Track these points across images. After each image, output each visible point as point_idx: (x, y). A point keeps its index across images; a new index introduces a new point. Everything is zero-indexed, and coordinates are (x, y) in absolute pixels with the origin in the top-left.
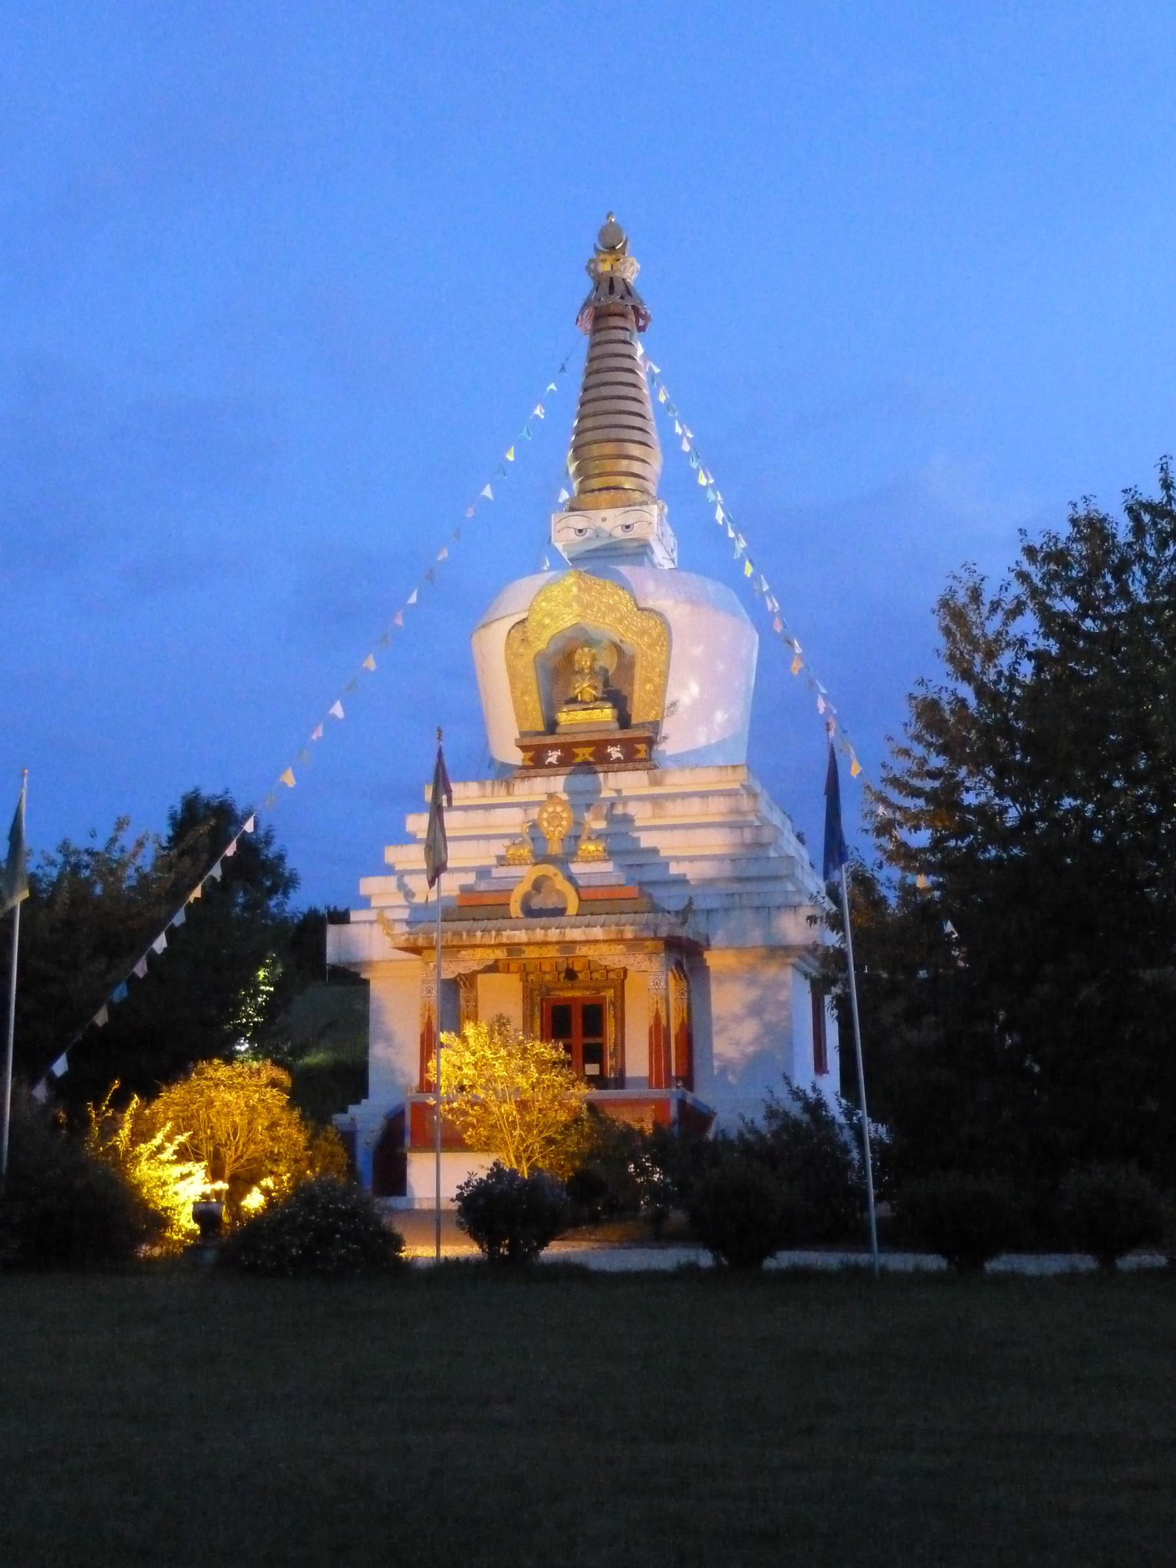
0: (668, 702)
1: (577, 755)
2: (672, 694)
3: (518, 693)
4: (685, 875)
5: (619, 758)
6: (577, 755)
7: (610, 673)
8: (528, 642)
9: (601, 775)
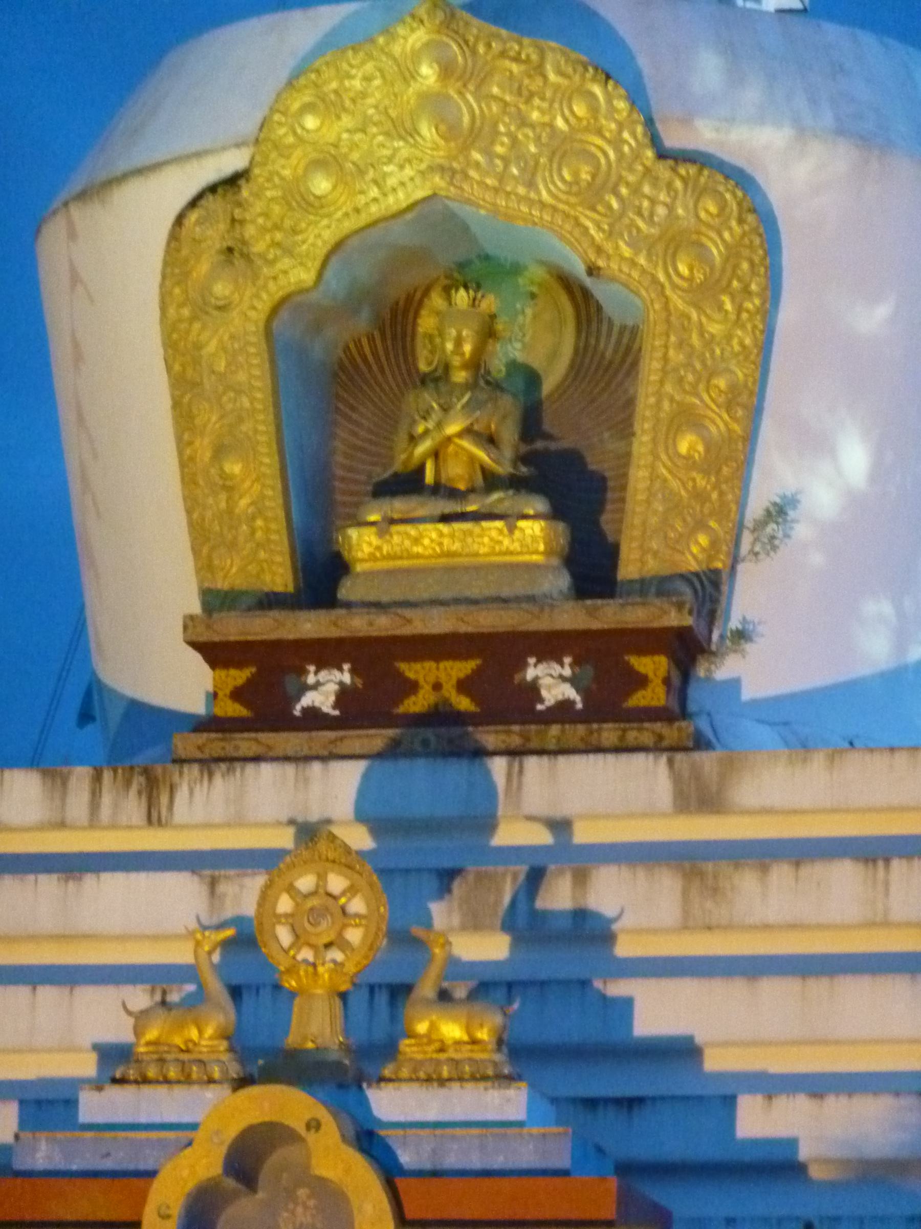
0: (755, 508)
1: (412, 687)
2: (775, 472)
3: (203, 449)
4: (792, 1143)
5: (565, 705)
6: (412, 687)
7: (548, 385)
8: (247, 258)
9: (498, 766)
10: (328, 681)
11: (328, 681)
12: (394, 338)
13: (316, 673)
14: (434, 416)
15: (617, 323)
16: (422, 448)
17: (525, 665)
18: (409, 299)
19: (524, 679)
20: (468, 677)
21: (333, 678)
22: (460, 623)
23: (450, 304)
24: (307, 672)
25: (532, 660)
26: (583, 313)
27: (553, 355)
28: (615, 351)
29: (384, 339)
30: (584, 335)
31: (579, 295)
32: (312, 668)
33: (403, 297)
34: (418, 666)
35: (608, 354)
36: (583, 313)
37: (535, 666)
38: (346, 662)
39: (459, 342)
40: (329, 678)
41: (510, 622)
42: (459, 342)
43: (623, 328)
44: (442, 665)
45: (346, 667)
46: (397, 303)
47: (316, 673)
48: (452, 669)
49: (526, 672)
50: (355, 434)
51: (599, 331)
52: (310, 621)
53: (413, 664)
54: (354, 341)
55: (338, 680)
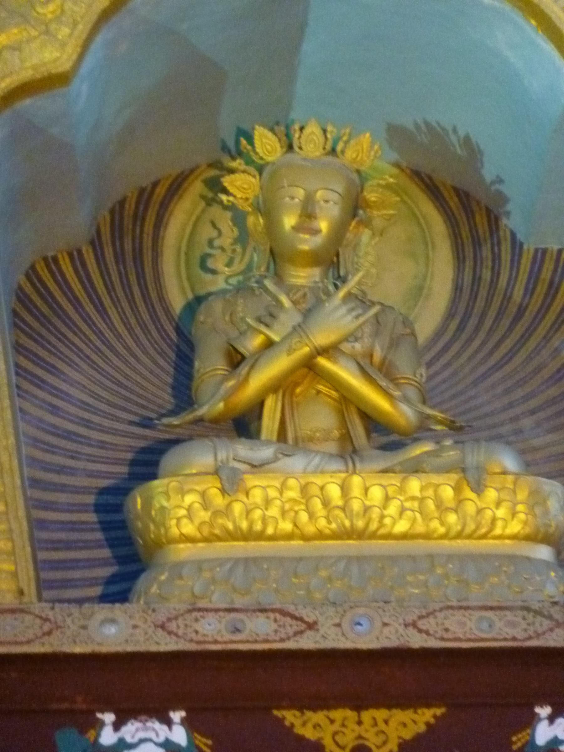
10: (142, 741)
11: (142, 741)
12: (119, 258)
13: (117, 726)
14: (283, 317)
15: (529, 247)
16: (260, 379)
17: (531, 720)
18: (144, 196)
19: (531, 742)
20: (418, 738)
21: (151, 735)
22: (411, 631)
23: (290, 148)
24: (102, 724)
25: (544, 711)
26: (465, 232)
27: (418, 292)
28: (530, 291)
29: (100, 259)
30: (469, 264)
31: (453, 202)
32: (109, 718)
33: (22, 279)
34: (319, 717)
35: (518, 294)
36: (465, 232)
37: (552, 719)
38: (175, 708)
39: (308, 213)
40: (142, 735)
41: (510, 632)
42: (308, 213)
43: (541, 254)
44: (367, 715)
45: (177, 716)
46: (122, 203)
47: (117, 726)
48: (386, 722)
49: (534, 730)
50: (55, 410)
51: (496, 258)
52: (113, 621)
53: (309, 714)
54: (45, 259)
55: (161, 739)
